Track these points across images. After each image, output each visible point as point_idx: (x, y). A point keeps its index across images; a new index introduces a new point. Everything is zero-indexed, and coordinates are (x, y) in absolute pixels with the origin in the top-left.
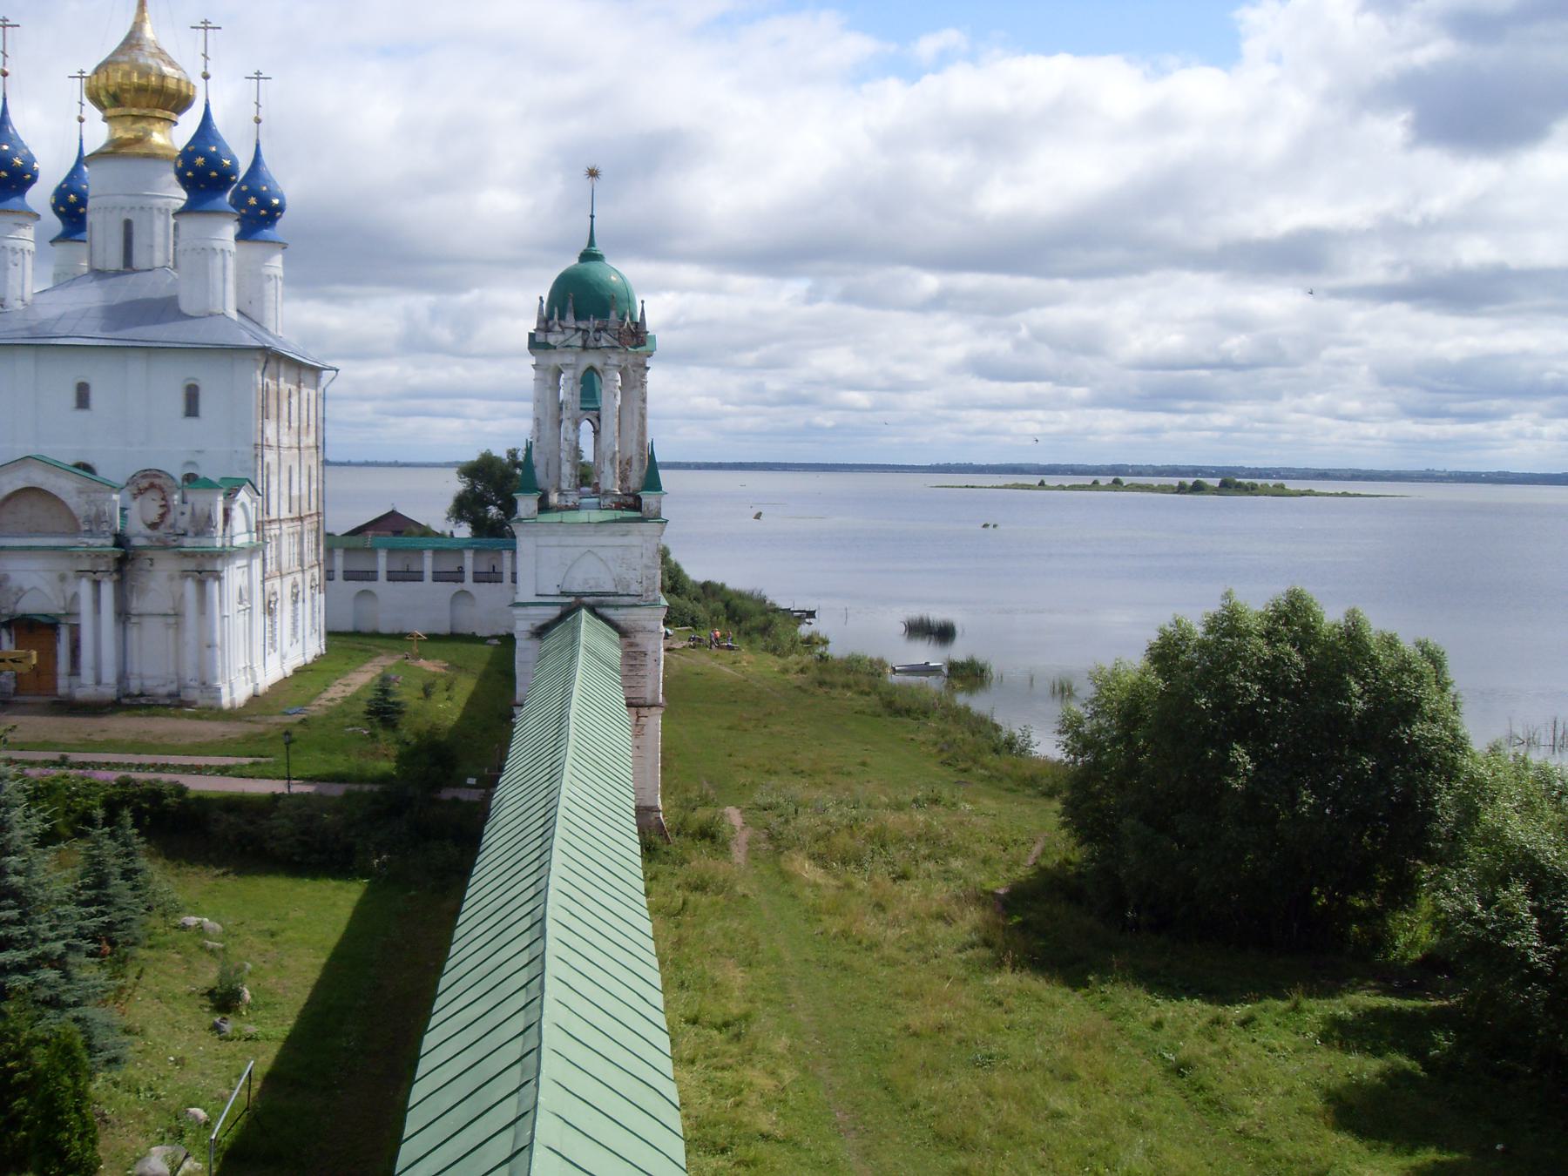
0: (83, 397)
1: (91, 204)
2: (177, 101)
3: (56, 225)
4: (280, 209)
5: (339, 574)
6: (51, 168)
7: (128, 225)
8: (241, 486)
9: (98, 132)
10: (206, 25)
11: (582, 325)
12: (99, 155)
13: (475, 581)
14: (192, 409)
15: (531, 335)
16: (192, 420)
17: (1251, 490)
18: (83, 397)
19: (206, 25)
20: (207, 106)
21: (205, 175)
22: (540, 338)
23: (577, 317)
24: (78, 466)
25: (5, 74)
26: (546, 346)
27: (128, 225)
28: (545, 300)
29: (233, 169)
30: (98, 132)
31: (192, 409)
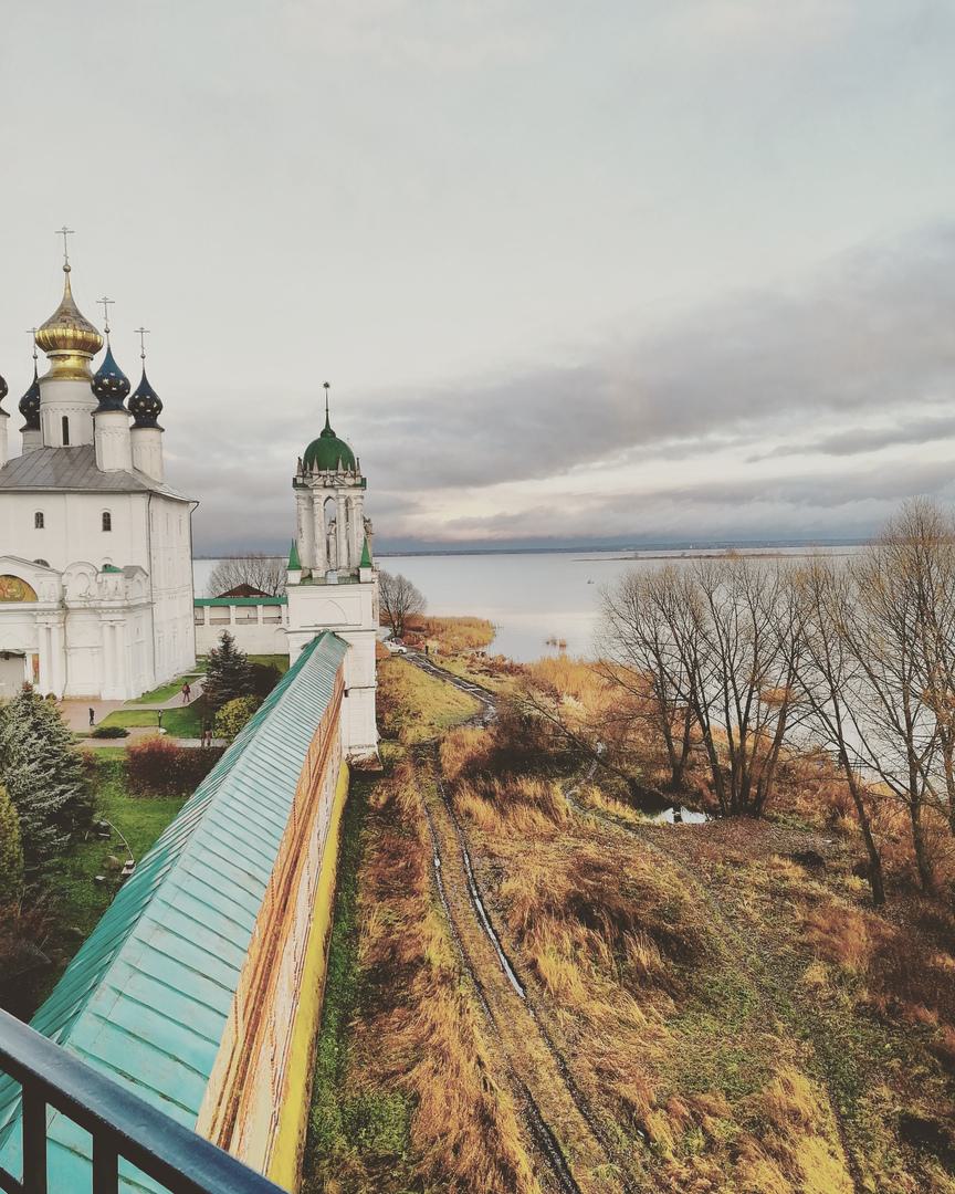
0: (39, 520)
1: (41, 407)
2: (95, 348)
3: (23, 421)
4: (160, 407)
5: (29, 659)
6: (18, 389)
7: (65, 420)
8: (137, 571)
9: (45, 366)
10: (105, 301)
11: (323, 473)
12: (45, 379)
13: (237, 623)
14: (107, 526)
15: (295, 480)
16: (108, 533)
17: (297, 858)
18: (39, 520)
19: (105, 301)
20: (109, 349)
21: (109, 390)
22: (300, 480)
23: (320, 469)
24: (38, 562)
25: (143, 357)
26: (304, 486)
27: (65, 420)
28: (302, 458)
29: (127, 386)
30: (45, 366)
31: (107, 526)
